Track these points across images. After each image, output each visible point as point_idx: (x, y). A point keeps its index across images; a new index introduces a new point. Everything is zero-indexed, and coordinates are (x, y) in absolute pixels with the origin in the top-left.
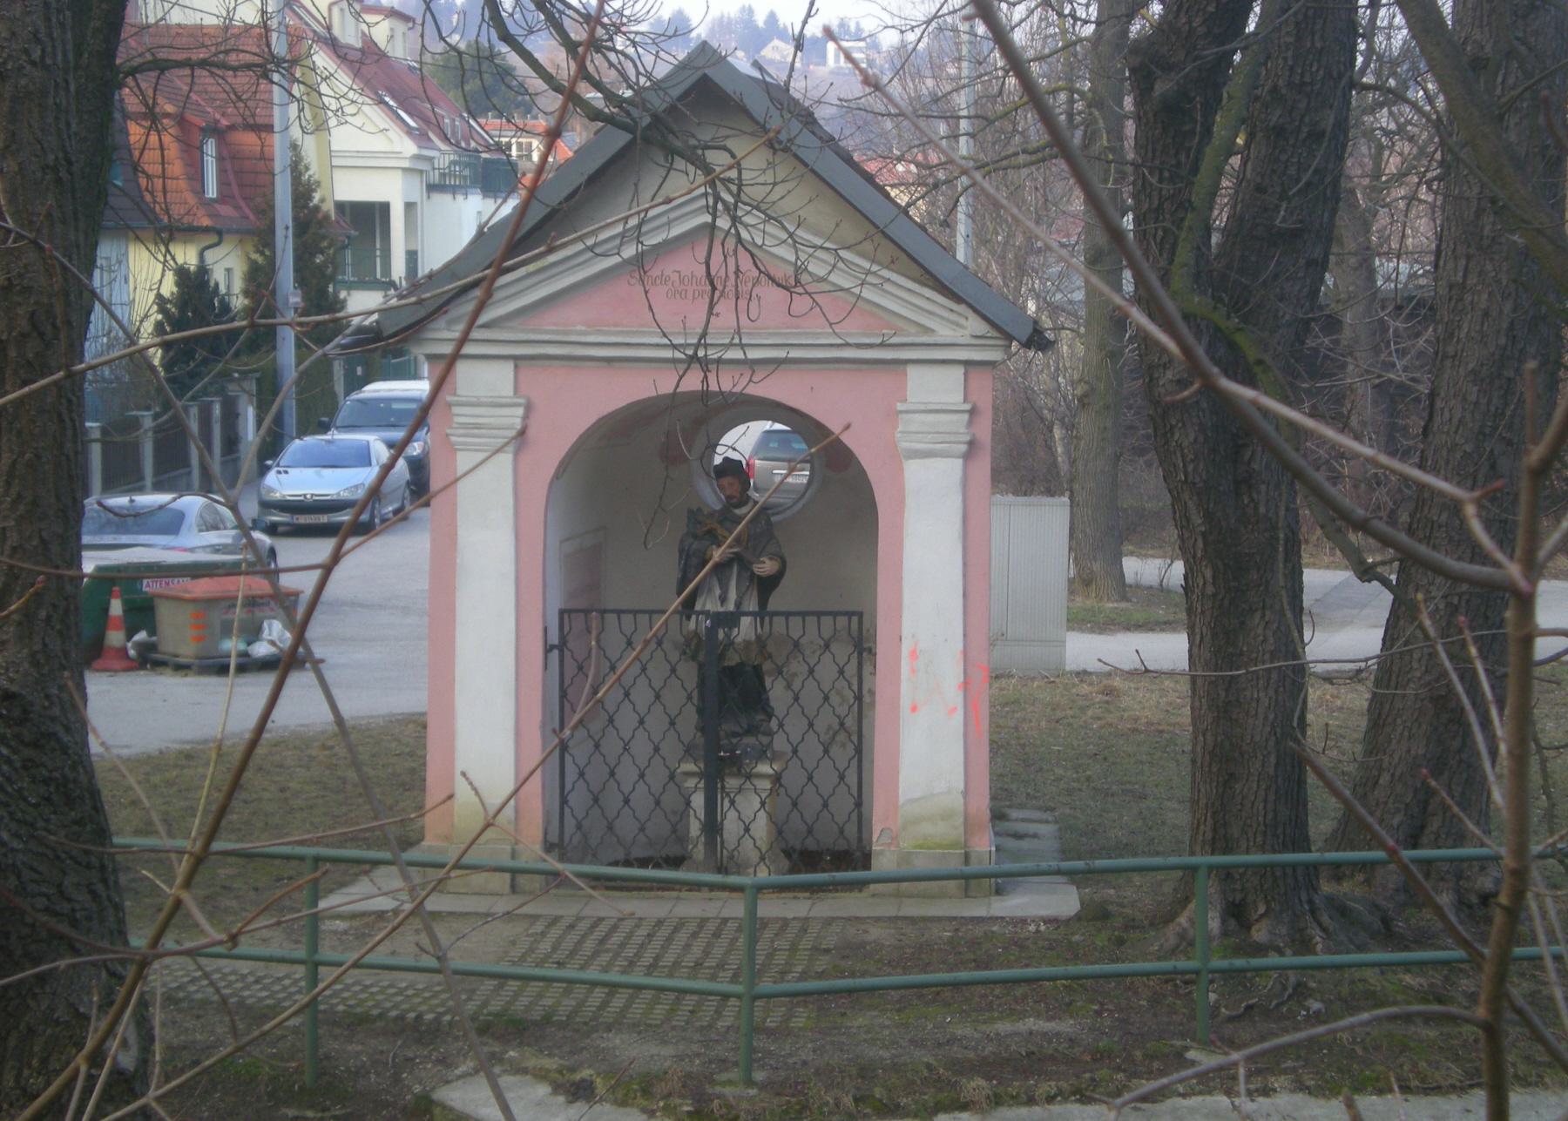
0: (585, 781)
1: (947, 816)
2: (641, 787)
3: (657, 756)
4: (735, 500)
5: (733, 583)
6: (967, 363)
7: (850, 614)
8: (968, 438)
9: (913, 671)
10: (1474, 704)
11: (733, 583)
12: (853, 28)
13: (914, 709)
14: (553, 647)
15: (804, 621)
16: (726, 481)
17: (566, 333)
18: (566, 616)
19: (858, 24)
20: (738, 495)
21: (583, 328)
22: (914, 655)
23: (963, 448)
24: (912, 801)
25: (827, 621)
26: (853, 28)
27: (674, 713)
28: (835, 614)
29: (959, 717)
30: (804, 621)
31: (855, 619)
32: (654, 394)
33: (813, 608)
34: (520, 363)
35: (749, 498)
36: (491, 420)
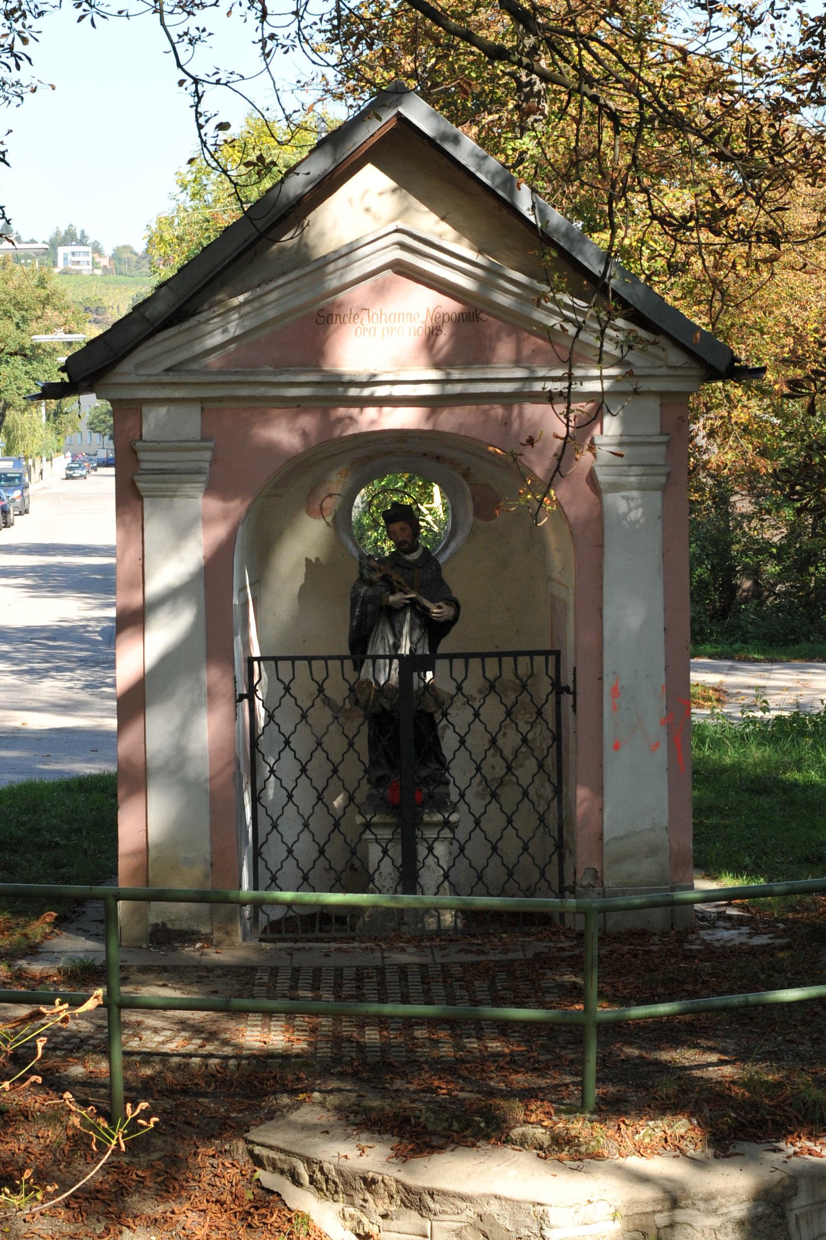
0: (546, 880)
1: (653, 851)
2: (337, 837)
3: (352, 804)
4: (406, 546)
5: (406, 629)
6: (661, 394)
7: (546, 653)
8: (665, 470)
9: (615, 708)
10: (21, 671)
11: (406, 629)
12: (79, 236)
13: (616, 747)
14: (242, 697)
15: (515, 661)
16: (396, 526)
17: (252, 374)
18: (256, 663)
19: (83, 232)
20: (409, 540)
21: (271, 369)
22: (615, 691)
23: (663, 479)
24: (617, 839)
25: (523, 661)
26: (79, 236)
27: (336, 759)
28: (515, 655)
29: (662, 753)
30: (515, 661)
31: (552, 659)
32: (113, 479)
33: (491, 649)
34: (207, 406)
35: (418, 545)
36: (151, 477)
